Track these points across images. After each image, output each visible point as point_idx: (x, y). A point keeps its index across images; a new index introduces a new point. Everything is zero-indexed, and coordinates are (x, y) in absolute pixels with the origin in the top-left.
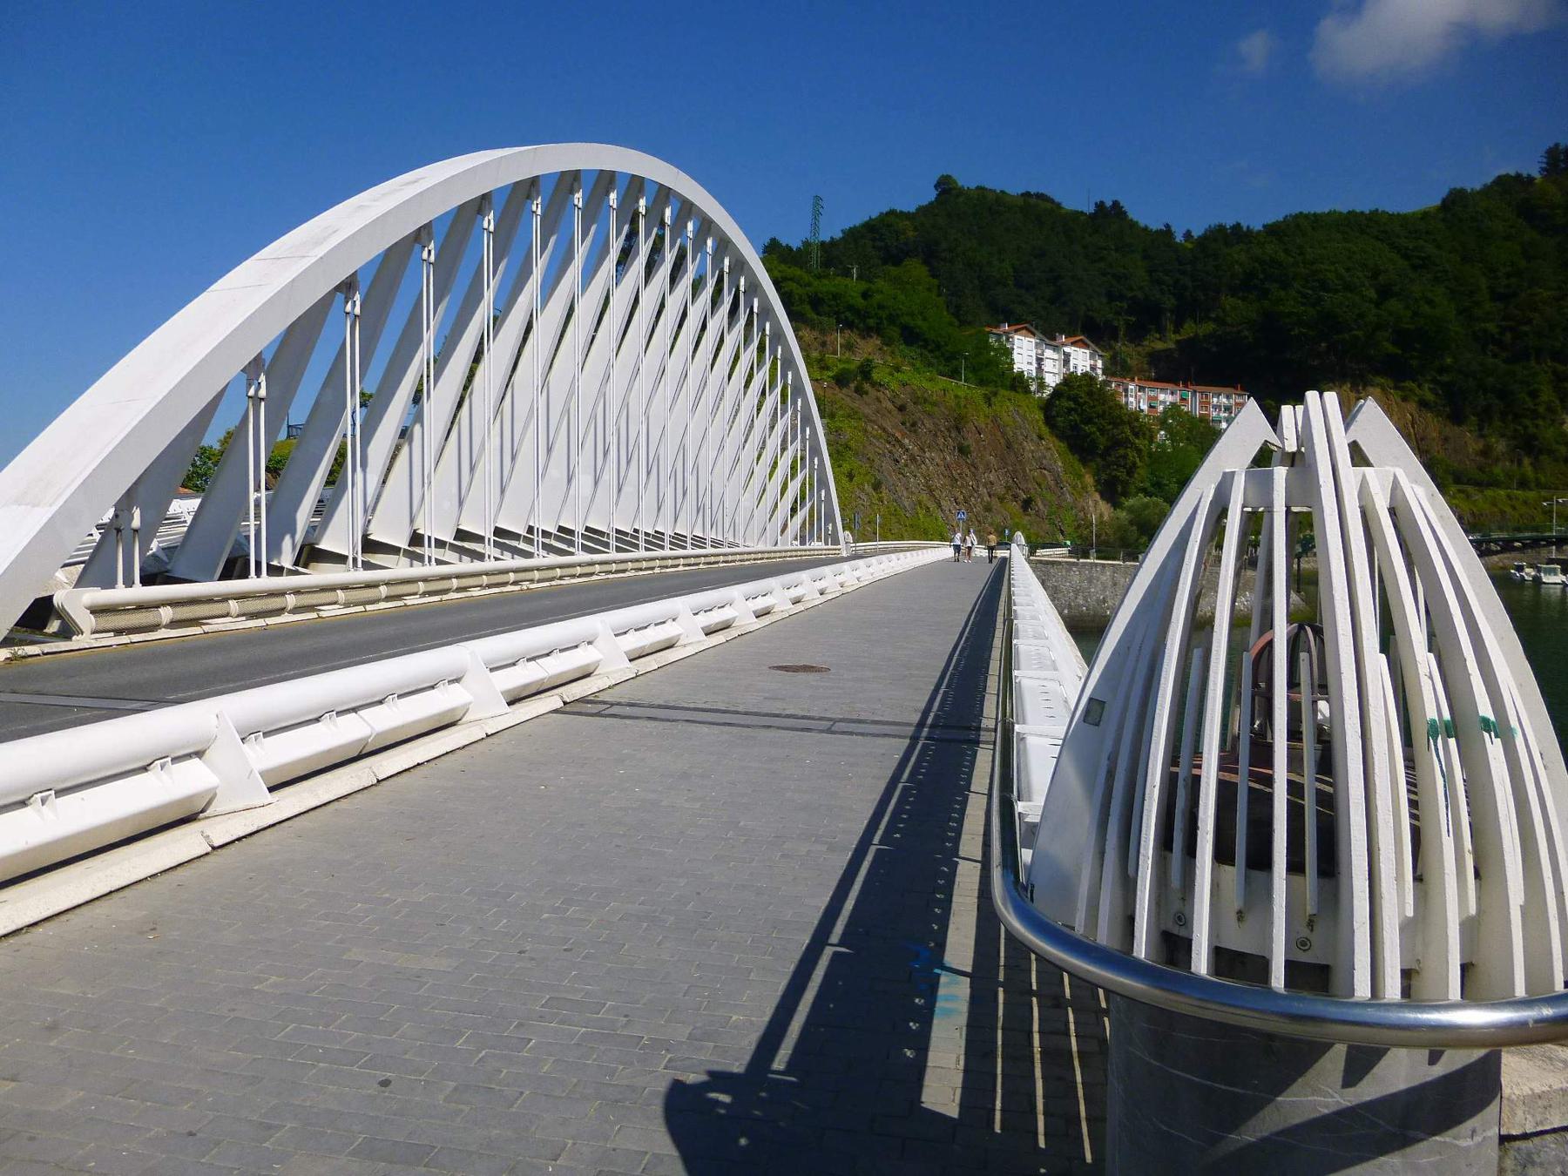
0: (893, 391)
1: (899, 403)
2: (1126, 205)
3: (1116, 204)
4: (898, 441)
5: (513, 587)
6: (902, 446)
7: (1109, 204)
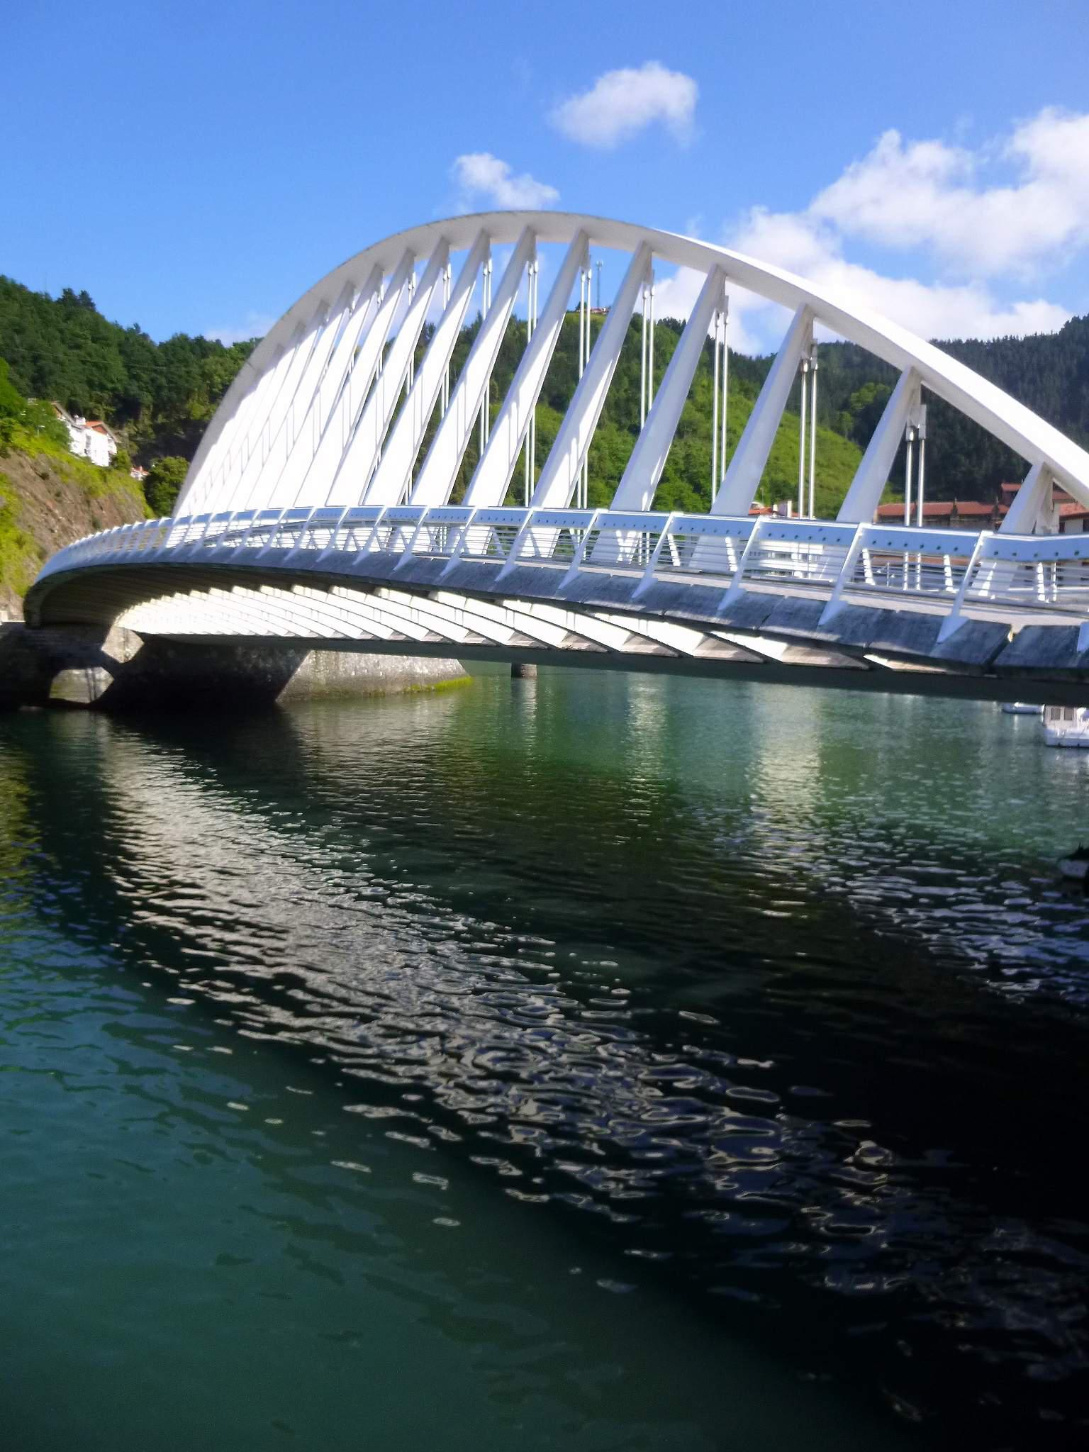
0: (34, 457)
1: (41, 471)
2: (95, 297)
3: (84, 294)
4: (50, 510)
5: (855, 550)
6: (54, 516)
7: (77, 293)
